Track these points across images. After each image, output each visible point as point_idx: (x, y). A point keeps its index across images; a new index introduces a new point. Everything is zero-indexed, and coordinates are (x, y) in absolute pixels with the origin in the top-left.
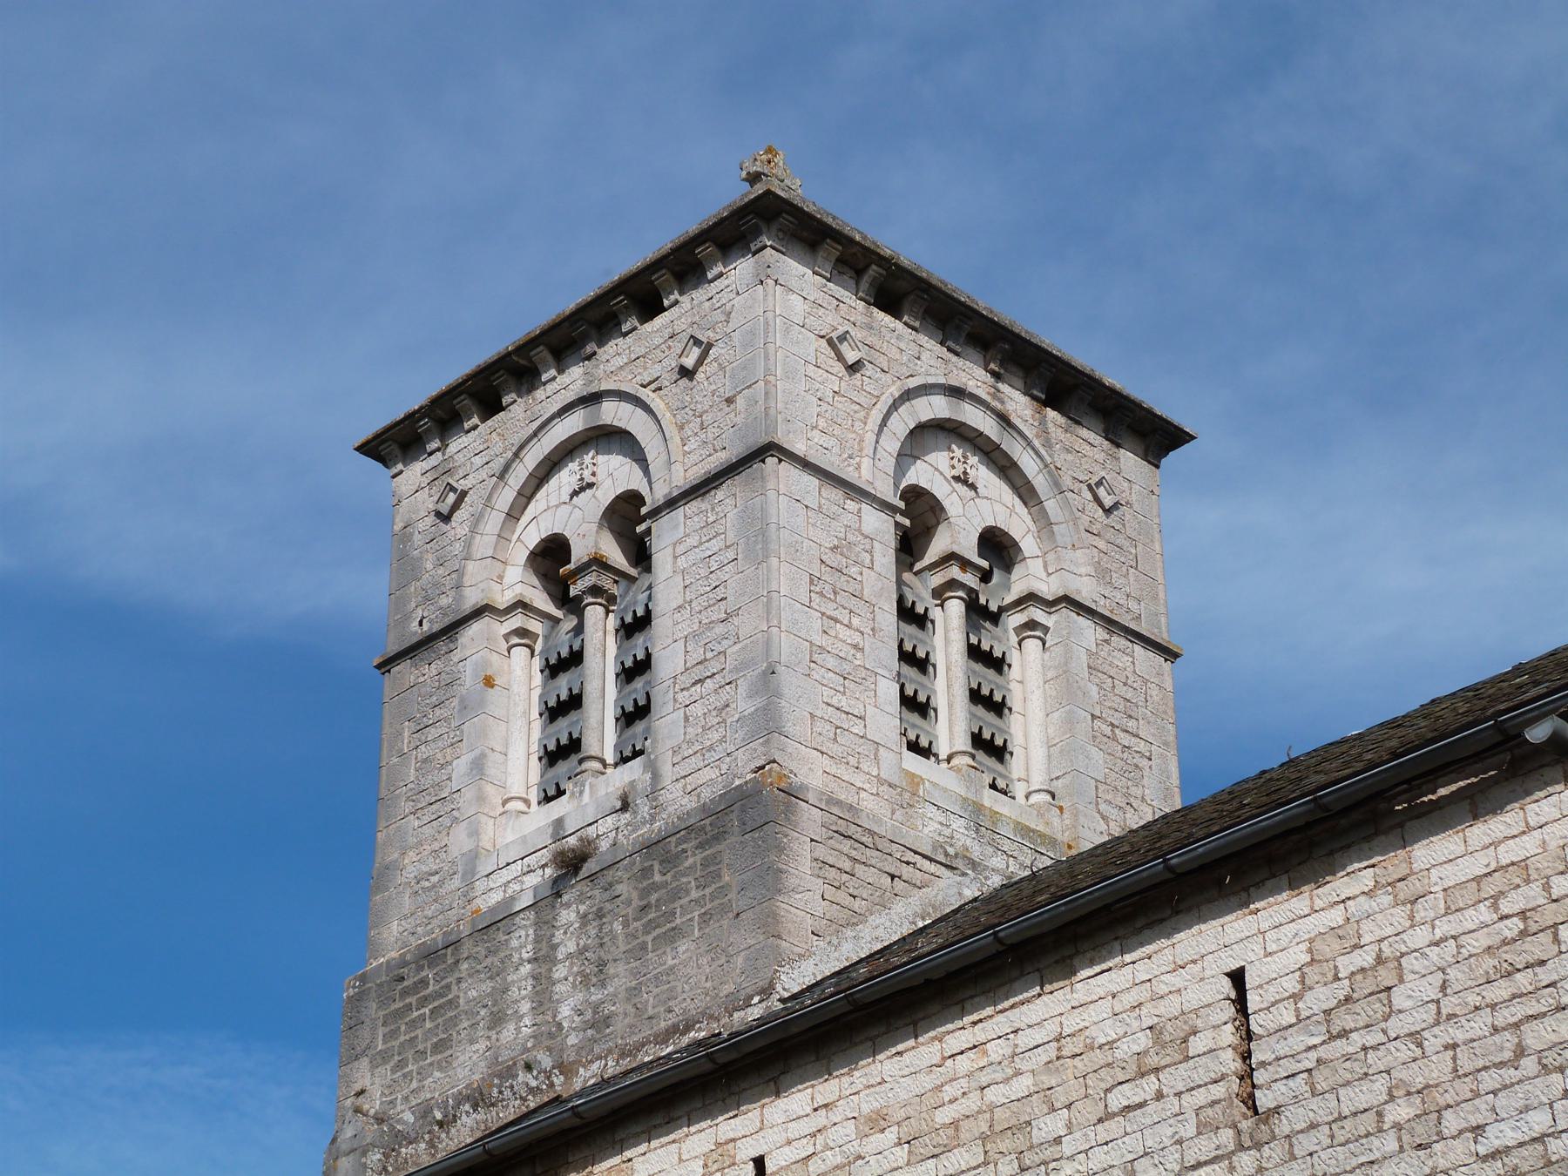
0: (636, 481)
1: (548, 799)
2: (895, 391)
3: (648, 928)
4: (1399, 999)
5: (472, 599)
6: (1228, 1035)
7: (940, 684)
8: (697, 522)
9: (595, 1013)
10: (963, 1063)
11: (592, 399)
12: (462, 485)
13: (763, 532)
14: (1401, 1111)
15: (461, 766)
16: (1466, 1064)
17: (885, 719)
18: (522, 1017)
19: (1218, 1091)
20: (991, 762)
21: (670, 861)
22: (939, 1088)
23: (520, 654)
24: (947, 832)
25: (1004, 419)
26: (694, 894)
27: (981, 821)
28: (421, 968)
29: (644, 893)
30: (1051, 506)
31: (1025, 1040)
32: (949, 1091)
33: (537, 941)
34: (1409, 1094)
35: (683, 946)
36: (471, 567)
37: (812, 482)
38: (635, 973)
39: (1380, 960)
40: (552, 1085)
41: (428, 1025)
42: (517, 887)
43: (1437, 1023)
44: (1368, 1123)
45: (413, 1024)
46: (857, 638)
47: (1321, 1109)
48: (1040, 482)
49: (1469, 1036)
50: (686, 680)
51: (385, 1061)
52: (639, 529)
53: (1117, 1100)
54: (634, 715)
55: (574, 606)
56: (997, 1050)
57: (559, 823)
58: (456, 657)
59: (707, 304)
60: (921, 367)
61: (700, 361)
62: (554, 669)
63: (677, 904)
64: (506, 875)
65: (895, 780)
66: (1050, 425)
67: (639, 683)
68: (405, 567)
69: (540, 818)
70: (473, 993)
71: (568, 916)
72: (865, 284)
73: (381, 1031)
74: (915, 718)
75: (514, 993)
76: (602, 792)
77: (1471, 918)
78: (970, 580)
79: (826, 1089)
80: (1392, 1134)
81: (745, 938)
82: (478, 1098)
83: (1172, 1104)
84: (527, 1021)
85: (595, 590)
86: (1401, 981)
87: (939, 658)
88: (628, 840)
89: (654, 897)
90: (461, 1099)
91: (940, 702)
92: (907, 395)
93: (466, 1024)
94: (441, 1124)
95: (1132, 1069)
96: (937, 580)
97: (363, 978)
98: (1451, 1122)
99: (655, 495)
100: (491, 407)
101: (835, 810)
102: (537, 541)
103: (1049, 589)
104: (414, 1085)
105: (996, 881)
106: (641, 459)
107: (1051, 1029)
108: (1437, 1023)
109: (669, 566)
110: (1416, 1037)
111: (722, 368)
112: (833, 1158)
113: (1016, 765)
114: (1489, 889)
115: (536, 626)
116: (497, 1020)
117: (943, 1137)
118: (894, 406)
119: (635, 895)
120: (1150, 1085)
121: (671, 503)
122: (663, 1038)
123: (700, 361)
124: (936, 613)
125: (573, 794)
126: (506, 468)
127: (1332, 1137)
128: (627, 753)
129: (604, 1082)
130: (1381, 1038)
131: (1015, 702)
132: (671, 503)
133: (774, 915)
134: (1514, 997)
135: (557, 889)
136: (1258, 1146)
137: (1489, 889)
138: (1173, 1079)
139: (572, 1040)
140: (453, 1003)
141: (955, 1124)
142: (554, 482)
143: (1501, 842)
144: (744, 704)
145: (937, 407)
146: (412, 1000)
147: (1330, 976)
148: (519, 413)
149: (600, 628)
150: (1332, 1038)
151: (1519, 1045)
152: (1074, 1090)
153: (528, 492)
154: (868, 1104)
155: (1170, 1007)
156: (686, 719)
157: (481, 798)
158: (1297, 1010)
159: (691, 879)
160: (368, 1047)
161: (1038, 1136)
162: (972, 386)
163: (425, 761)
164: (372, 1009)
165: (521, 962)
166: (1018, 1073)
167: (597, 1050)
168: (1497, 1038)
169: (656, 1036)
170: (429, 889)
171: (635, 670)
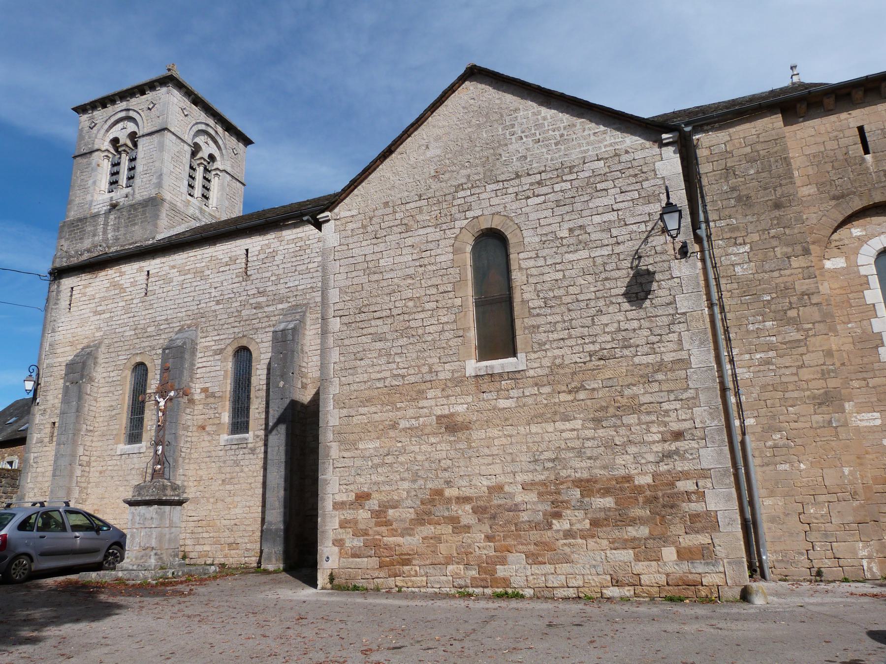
0: (136, 129)
1: (109, 192)
2: (194, 122)
3: (130, 222)
4: (276, 258)
5: (96, 147)
6: (244, 260)
7: (197, 183)
8: (149, 141)
10: (192, 259)
11: (128, 110)
12: (96, 122)
13: (163, 146)
14: (273, 278)
15: (90, 182)
16: (286, 272)
17: (184, 188)
19: (241, 270)
20: (205, 200)
21: (135, 209)
23: (106, 161)
25: (216, 132)
27: (201, 211)
29: (129, 215)
30: (224, 151)
31: (205, 256)
32: (189, 263)
36: (96, 140)
37: (175, 137)
38: (126, 230)
45: (75, 234)
48: (222, 146)
50: (142, 173)
53: (221, 269)
54: (131, 178)
55: (119, 153)
56: (199, 257)
57: (112, 198)
58: (91, 158)
60: (200, 118)
61: (153, 107)
62: (114, 165)
64: (98, 206)
67: (132, 172)
68: (81, 137)
71: (112, 217)
72: (191, 98)
74: (191, 189)
76: (122, 193)
77: (291, 246)
78: (205, 163)
79: (164, 260)
81: (150, 227)
82: (89, 251)
83: (232, 272)
85: (124, 151)
87: (197, 178)
88: (126, 204)
90: (85, 250)
91: (196, 186)
92: (197, 123)
96: (199, 162)
97: (64, 222)
98: (282, 281)
99: (140, 133)
100: (104, 106)
103: (221, 168)
105: (203, 223)
106: (137, 125)
107: (210, 254)
110: (278, 266)
112: (164, 273)
113: (210, 201)
114: (295, 241)
115: (110, 155)
116: (94, 235)
117: (186, 272)
118: (194, 125)
120: (228, 268)
121: (143, 136)
122: (130, 244)
123: (153, 107)
124: (197, 169)
126: (107, 121)
129: (117, 251)
131: (212, 189)
132: (143, 136)
133: (156, 224)
135: (110, 211)
137: (295, 241)
138: (233, 267)
139: (111, 242)
140: (84, 231)
141: (189, 270)
142: (117, 126)
144: (155, 180)
145: (203, 127)
148: (110, 109)
149: (125, 160)
152: (213, 266)
154: (172, 263)
157: (95, 189)
161: (205, 274)
162: (211, 124)
164: (66, 229)
171: (132, 169)
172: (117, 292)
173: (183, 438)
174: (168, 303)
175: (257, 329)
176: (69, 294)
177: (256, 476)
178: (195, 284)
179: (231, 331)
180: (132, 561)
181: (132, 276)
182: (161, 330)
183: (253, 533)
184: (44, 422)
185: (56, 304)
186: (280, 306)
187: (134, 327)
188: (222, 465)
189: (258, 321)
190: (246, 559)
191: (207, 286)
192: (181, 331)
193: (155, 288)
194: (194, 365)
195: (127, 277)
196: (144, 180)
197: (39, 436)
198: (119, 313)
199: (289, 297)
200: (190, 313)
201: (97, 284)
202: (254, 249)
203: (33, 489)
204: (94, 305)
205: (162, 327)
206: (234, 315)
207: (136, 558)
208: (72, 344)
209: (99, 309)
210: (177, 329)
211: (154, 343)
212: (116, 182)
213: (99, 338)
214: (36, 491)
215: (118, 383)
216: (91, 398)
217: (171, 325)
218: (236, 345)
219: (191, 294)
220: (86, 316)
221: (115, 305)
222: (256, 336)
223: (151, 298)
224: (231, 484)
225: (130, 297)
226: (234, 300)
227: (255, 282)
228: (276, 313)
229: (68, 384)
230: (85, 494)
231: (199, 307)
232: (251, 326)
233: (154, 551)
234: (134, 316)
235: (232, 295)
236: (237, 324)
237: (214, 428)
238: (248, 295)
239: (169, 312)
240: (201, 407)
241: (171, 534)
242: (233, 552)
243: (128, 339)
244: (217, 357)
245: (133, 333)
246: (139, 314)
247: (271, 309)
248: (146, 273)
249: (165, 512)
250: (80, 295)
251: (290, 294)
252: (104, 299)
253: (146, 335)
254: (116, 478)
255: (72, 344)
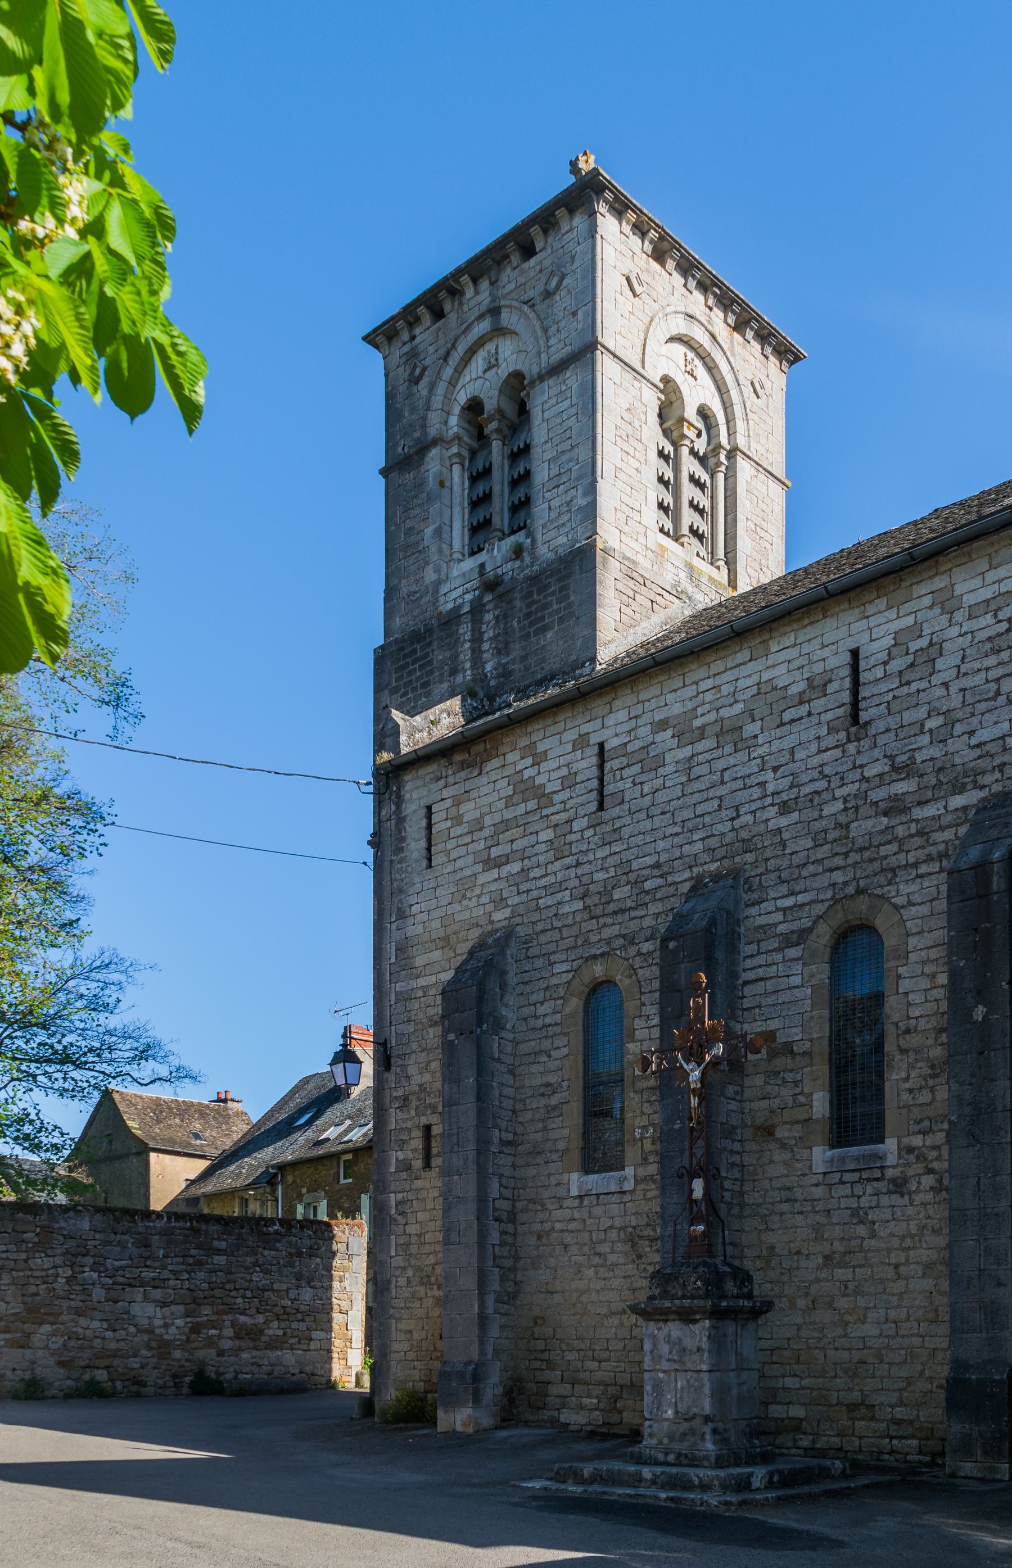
1: (473, 553)
3: (531, 624)
4: (940, 664)
9: (504, 669)
10: (709, 697)
16: (969, 699)
18: (466, 671)
22: (695, 709)
24: (677, 579)
26: (555, 607)
28: (413, 644)
33: (473, 630)
34: (938, 714)
35: (550, 635)
38: (524, 648)
39: (931, 644)
40: (483, 706)
41: (418, 674)
42: (461, 601)
43: (957, 677)
44: (915, 729)
45: (410, 673)
46: (637, 464)
47: (892, 722)
49: (973, 684)
51: (397, 692)
52: (523, 394)
53: (787, 716)
56: (726, 689)
57: (482, 566)
59: (561, 250)
63: (546, 612)
65: (654, 549)
66: (735, 343)
69: (470, 564)
70: (440, 657)
73: (394, 676)
75: (462, 657)
80: (928, 735)
83: (815, 719)
84: (469, 672)
86: (941, 655)
89: (534, 608)
93: (437, 674)
94: (432, 722)
95: (796, 700)
98: (958, 729)
101: (626, 563)
102: (465, 400)
104: (412, 704)
108: (957, 677)
109: (540, 417)
110: (946, 685)
111: (569, 292)
114: (993, 606)
116: (454, 672)
119: (524, 607)
120: (804, 709)
125: (488, 550)
127: (897, 736)
128: (515, 528)
130: (927, 685)
132: (541, 378)
134: (999, 664)
136: (858, 740)
137: (993, 606)
138: (818, 705)
139: (493, 683)
140: (431, 662)
143: (1003, 580)
146: (409, 660)
147: (904, 652)
150: (901, 685)
151: (999, 689)
153: (459, 370)
155: (818, 668)
156: (550, 508)
158: (885, 670)
159: (553, 598)
160: (388, 684)
163: (409, 529)
165: (465, 641)
166: (736, 702)
167: (505, 688)
168: (987, 686)
169: (536, 682)
170: (415, 601)
172: (532, 805)
173: (725, 1155)
174: (657, 822)
175: (893, 870)
176: (424, 823)
177: (909, 1249)
178: (720, 764)
179: (825, 880)
180: (661, 1443)
181: (563, 761)
182: (647, 892)
183: (910, 1384)
184: (409, 1124)
185: (401, 850)
186: (958, 801)
187: (582, 890)
188: (821, 1219)
189: (894, 848)
190: (895, 1442)
191: (754, 766)
192: (698, 887)
193: (621, 785)
194: (735, 976)
195: (552, 764)
196: (555, 503)
197: (401, 1155)
198: (542, 859)
199: (983, 773)
200: (713, 843)
201: (484, 790)
202: (876, 646)
203: (404, 1269)
204: (482, 845)
205: (648, 885)
206: (831, 836)
207: (671, 1438)
208: (445, 942)
209: (495, 852)
210: (686, 887)
211: (633, 926)
212: (487, 522)
213: (505, 923)
214: (410, 1273)
215: (558, 1029)
216: (503, 1068)
217: (670, 879)
218: (838, 918)
219: (711, 793)
220: (468, 872)
221: (533, 839)
222: (892, 888)
223: (615, 812)
224: (846, 1265)
225: (564, 816)
226: (826, 796)
227: (881, 740)
228: (944, 822)
229: (451, 1037)
230: (511, 1283)
231: (737, 823)
232: (876, 865)
233: (711, 1425)
234: (578, 864)
235: (822, 784)
236: (838, 861)
237: (797, 1131)
238: (864, 779)
239: (661, 845)
240: (759, 1080)
241: (740, 1384)
242: (859, 1424)
243: (570, 921)
244: (793, 952)
245: (579, 905)
246: (591, 857)
247: (931, 811)
248: (596, 750)
249: (725, 1335)
250: (449, 824)
251: (985, 763)
252: (505, 825)
253: (612, 907)
254: (575, 1249)
255: (445, 942)
